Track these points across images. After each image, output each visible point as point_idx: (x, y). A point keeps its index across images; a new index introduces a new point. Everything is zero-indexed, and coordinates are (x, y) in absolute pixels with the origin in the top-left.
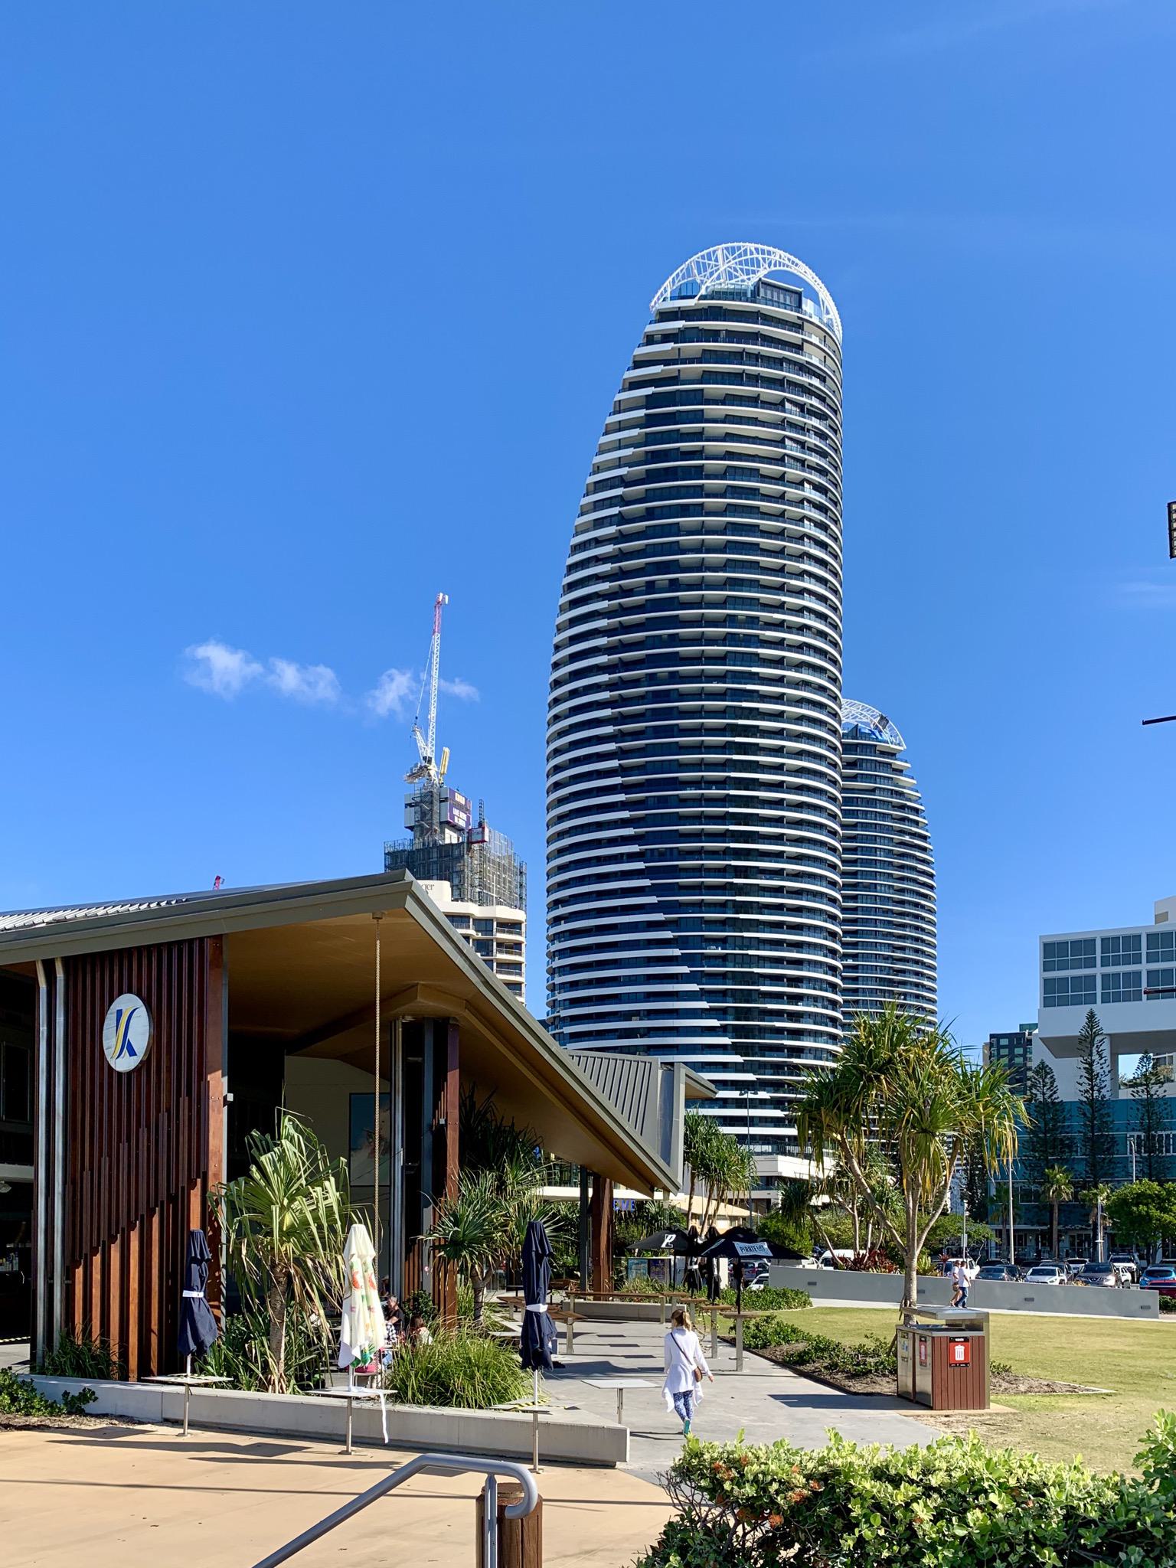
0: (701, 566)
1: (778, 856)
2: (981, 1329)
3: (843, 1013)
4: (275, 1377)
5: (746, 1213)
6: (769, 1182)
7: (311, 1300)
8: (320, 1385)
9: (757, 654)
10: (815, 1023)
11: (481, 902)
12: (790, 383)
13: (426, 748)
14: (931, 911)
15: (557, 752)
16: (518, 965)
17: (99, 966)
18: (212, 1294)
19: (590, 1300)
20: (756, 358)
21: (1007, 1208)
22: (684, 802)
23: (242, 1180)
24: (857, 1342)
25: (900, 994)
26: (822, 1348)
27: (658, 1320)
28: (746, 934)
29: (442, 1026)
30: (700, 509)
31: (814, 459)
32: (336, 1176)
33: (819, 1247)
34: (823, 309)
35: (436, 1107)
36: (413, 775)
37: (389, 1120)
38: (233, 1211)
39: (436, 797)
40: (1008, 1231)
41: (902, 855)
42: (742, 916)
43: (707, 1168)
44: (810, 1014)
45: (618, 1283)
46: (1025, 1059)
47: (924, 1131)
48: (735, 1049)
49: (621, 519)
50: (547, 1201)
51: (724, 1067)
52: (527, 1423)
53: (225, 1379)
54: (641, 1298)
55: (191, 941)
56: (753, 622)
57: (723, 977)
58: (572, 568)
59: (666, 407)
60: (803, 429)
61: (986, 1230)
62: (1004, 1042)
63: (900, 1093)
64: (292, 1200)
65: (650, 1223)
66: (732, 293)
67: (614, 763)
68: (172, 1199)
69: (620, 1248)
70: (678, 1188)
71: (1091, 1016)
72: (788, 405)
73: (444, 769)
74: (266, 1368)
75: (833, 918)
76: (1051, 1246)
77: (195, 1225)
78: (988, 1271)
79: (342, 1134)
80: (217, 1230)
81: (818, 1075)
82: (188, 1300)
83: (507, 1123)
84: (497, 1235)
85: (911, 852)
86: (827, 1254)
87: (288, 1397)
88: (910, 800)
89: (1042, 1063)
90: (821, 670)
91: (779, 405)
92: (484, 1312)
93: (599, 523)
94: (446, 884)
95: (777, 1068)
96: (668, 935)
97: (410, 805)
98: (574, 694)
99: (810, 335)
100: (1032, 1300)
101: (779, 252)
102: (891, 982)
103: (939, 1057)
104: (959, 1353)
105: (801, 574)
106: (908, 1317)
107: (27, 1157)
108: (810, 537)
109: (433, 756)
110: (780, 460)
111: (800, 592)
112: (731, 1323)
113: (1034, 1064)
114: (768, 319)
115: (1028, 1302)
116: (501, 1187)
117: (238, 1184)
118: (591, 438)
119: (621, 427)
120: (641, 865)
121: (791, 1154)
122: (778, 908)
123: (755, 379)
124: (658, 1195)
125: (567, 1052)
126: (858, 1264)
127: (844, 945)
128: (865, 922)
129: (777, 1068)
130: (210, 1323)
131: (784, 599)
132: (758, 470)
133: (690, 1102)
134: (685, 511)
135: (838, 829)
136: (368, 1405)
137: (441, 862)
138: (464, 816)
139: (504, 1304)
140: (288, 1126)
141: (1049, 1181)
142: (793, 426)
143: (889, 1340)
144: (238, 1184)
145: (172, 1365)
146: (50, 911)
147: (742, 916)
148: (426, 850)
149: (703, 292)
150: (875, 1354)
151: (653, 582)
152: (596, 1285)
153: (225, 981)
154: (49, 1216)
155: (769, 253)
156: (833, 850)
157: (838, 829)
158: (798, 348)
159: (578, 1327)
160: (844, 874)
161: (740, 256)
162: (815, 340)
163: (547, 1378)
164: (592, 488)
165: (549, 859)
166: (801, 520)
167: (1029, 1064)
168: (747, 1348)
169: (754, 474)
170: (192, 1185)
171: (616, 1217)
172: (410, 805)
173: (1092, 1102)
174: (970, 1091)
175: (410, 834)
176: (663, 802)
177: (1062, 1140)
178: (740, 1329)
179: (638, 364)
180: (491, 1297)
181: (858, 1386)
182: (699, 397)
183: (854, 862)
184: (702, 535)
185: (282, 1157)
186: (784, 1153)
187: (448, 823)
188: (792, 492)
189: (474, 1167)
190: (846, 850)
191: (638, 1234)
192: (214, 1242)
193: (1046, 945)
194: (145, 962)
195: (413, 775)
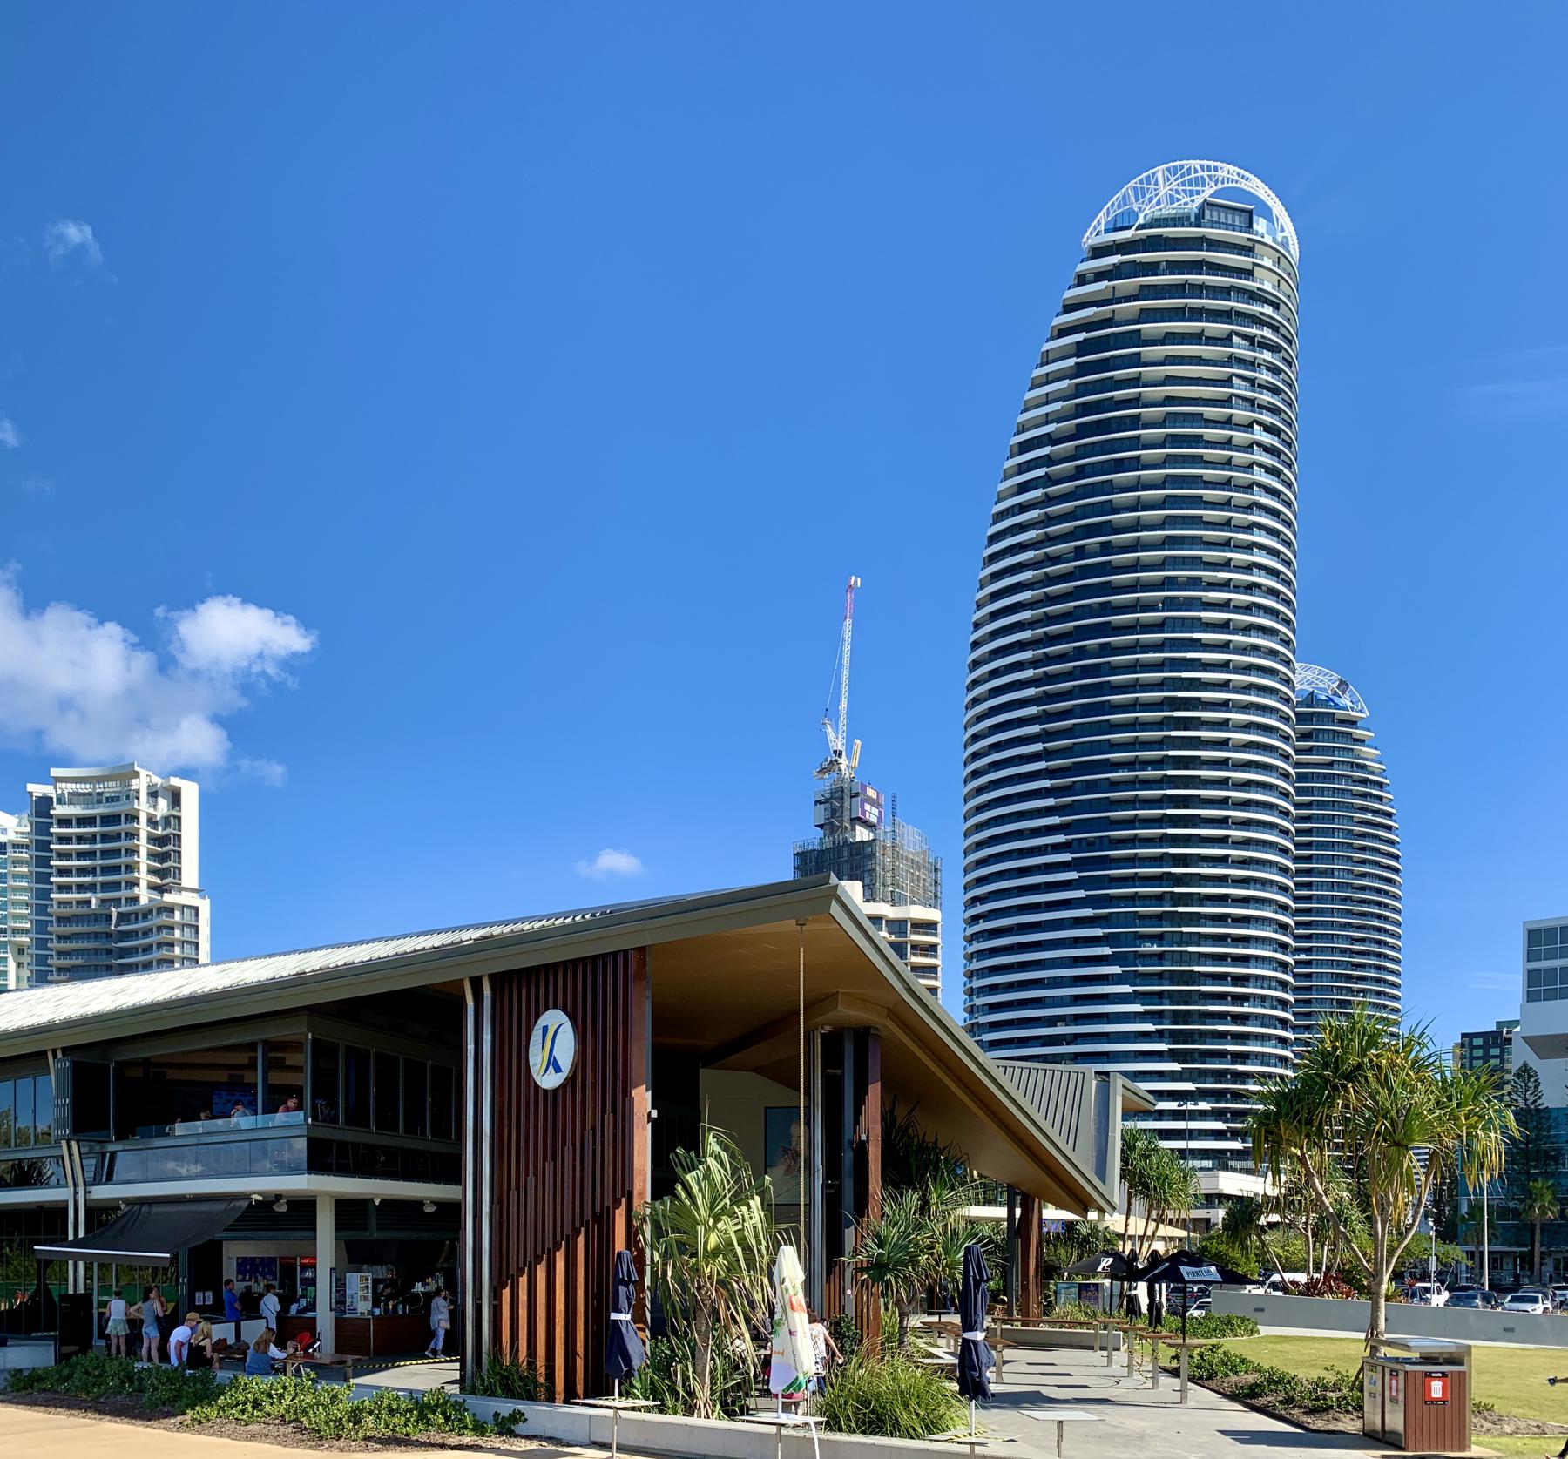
0: (1137, 526)
2: (1462, 1364)
3: (1294, 1014)
4: (701, 1402)
5: (1184, 1234)
6: (1212, 1199)
7: (736, 1322)
8: (745, 1410)
9: (1200, 619)
10: (1262, 1026)
11: (895, 901)
12: (1238, 313)
13: (837, 741)
14: (1395, 897)
15: (976, 738)
16: (934, 969)
17: (525, 980)
18: (638, 1317)
19: (1018, 1326)
20: (1200, 290)
21: (1481, 1223)
22: (1115, 785)
23: (667, 1199)
24: (1314, 1374)
25: (1359, 991)
26: (1276, 1380)
27: (1091, 1348)
28: (1185, 929)
29: (863, 1036)
30: (1136, 464)
31: (1265, 397)
32: (762, 1195)
33: (1268, 1271)
34: (1279, 228)
35: (857, 1122)
36: (822, 771)
37: (809, 1136)
38: (658, 1232)
40: (1482, 1253)
41: (1363, 836)
42: (1181, 909)
43: (1146, 1186)
44: (1257, 1016)
45: (1048, 1308)
46: (1503, 1061)
47: (1397, 1144)
48: (1172, 1056)
49: (1048, 480)
50: (972, 1222)
51: (1161, 1075)
52: (963, 1455)
53: (652, 1403)
54: (1074, 1324)
55: (615, 954)
56: (1194, 583)
57: (1160, 977)
58: (993, 539)
59: (1100, 351)
60: (1253, 364)
61: (1457, 1252)
62: (1478, 1042)
63: (1369, 1102)
64: (717, 1219)
65: (1081, 1246)
66: (1173, 219)
67: (1038, 747)
68: (597, 1219)
69: (1049, 1271)
70: (1114, 1208)
73: (855, 763)
74: (691, 1394)
75: (1284, 908)
76: (1531, 1269)
77: (620, 1245)
78: (1458, 1297)
79: (766, 1149)
80: (641, 1252)
81: (1276, 1084)
82: (615, 1321)
83: (930, 1139)
84: (923, 1258)
85: (1373, 833)
86: (1276, 1278)
87: (713, 1422)
88: (1373, 773)
89: (1525, 1065)
91: (1226, 340)
92: (909, 1338)
93: (1024, 488)
94: (858, 884)
97: (820, 802)
98: (995, 674)
100: (1512, 1330)
102: (1349, 978)
103: (1415, 1062)
104: (1436, 1389)
106: (1374, 1349)
107: (456, 1178)
109: (843, 749)
110: (1225, 402)
111: (1248, 547)
112: (1172, 1352)
113: (1514, 1065)
114: (1214, 245)
115: (1508, 1333)
116: (924, 1207)
117: (663, 1204)
118: (1017, 388)
119: (1048, 379)
120: (1067, 857)
121: (1234, 1170)
123: (1198, 314)
124: (1092, 1216)
125: (986, 1058)
126: (1311, 1289)
127: (1296, 938)
128: (1320, 912)
129: (1220, 1076)
130: (639, 1345)
131: (1230, 555)
133: (1126, 1116)
134: (1119, 466)
135: (1291, 809)
136: (801, 1433)
137: (857, 862)
138: (875, 811)
139: (928, 1328)
140: (712, 1144)
141: (1530, 1196)
142: (1241, 362)
143: (1353, 1373)
144: (663, 1204)
145: (598, 1387)
146: (476, 927)
147: (1181, 909)
148: (837, 849)
149: (1141, 221)
150: (1336, 1388)
152: (1025, 1311)
153: (649, 994)
154: (477, 1238)
155: (1216, 169)
156: (1285, 832)
157: (1291, 809)
158: (1248, 274)
159: (1008, 1354)
160: (1297, 859)
161: (1183, 176)
162: (1267, 262)
163: (984, 1408)
164: (1016, 449)
165: (966, 853)
166: (1249, 467)
167: (1507, 1066)
168: (1192, 1379)
169: (1198, 419)
170: (617, 1204)
171: (1043, 1239)
172: (820, 802)
174: (1450, 1100)
175: (820, 833)
176: (1092, 787)
177: (1546, 1152)
178: (1184, 1359)
179: (1068, 308)
180: (915, 1321)
181: (1318, 1423)
182: (1136, 339)
183: (1309, 845)
184: (1137, 495)
185: (708, 1175)
186: (1226, 1168)
188: (1240, 436)
189: (896, 1187)
190: (1299, 832)
191: (1066, 1256)
192: (639, 1261)
193: (1530, 932)
194: (570, 975)
195: (822, 771)
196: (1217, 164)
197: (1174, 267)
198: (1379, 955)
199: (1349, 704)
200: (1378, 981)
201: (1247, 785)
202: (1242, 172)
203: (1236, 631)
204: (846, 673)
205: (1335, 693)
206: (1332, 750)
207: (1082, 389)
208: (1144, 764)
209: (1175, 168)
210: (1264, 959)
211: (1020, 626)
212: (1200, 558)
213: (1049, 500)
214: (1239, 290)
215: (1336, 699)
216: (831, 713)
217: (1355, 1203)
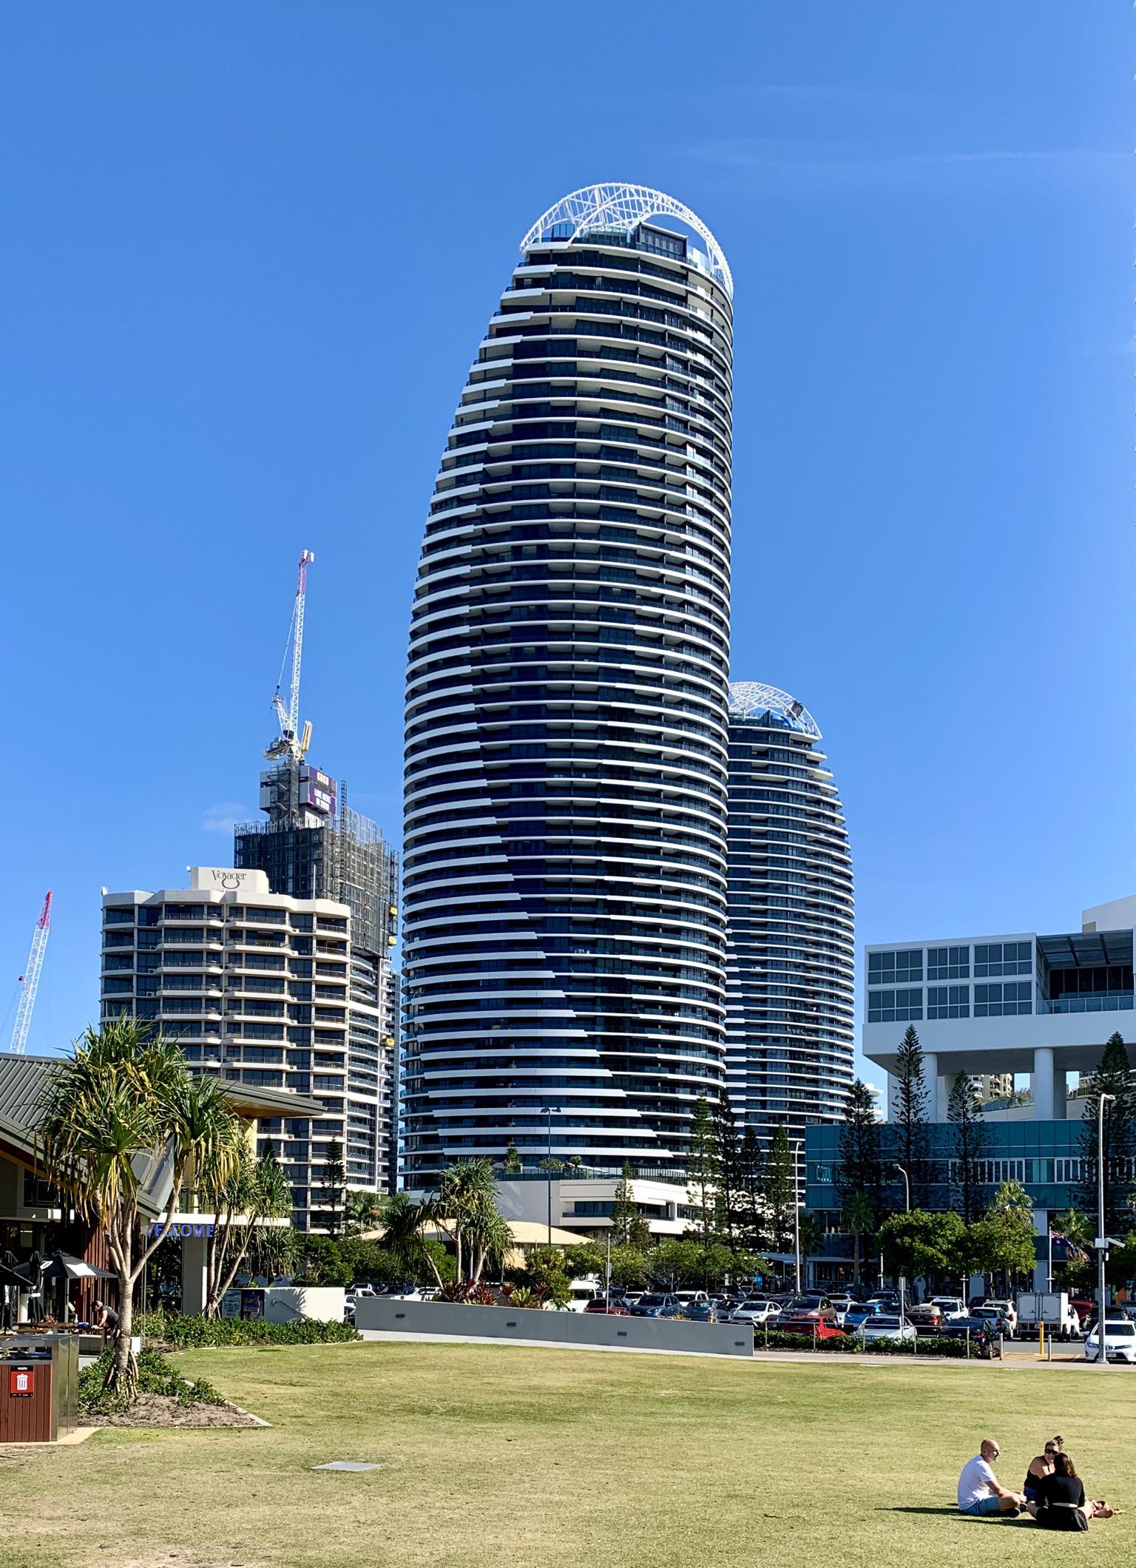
0: (572, 532)
1: (654, 852)
9: (634, 631)
12: (672, 337)
14: (848, 916)
15: (415, 730)
20: (635, 309)
28: (617, 937)
30: (572, 471)
31: (700, 421)
34: (709, 259)
36: (272, 751)
39: (294, 776)
41: (817, 854)
42: (613, 917)
51: (592, 1082)
56: (628, 595)
59: (534, 356)
60: (686, 387)
71: (911, 1033)
72: (668, 361)
88: (826, 795)
90: (703, 651)
91: (660, 361)
93: (461, 480)
95: (652, 1083)
96: (532, 936)
97: (266, 784)
98: (433, 666)
99: (695, 286)
101: (661, 195)
102: (803, 993)
104: (22, 1382)
105: (682, 546)
108: (693, 505)
110: (659, 421)
111: (682, 565)
115: (511, 1328)
118: (440, 384)
119: (486, 376)
122: (653, 910)
123: (632, 332)
132: (635, 430)
134: (555, 471)
138: (327, 798)
142: (675, 384)
147: (613, 917)
148: (280, 836)
149: (577, 234)
151: (520, 547)
158: (682, 300)
161: (619, 197)
162: (701, 291)
164: (454, 441)
166: (682, 486)
172: (266, 784)
173: (907, 1126)
176: (529, 790)
179: (506, 309)
182: (571, 348)
184: (573, 497)
186: (636, 1177)
187: (308, 805)
195: (272, 751)
196: (652, 191)
197: (610, 284)
198: (831, 971)
200: (831, 996)
201: (679, 799)
202: (676, 202)
204: (298, 650)
205: (790, 715)
206: (785, 770)
207: (519, 390)
208: (579, 771)
209: (611, 188)
214: (673, 314)
215: (790, 720)
216: (281, 691)
217: (441, 1221)
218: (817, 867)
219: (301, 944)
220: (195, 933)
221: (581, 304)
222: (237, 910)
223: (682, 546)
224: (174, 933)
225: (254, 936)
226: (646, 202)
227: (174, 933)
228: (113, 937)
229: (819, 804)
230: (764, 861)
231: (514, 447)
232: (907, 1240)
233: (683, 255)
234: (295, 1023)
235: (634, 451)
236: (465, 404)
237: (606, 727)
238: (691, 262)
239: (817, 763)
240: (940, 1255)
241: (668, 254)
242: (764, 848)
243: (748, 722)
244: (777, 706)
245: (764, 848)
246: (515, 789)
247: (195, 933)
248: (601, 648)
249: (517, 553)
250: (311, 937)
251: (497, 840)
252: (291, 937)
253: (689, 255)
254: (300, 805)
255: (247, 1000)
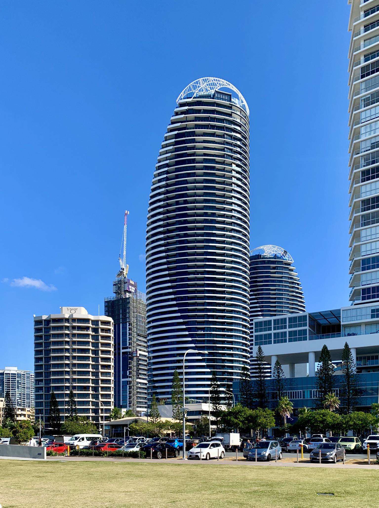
1: (223, 298)
20: (213, 119)
30: (194, 175)
34: (240, 101)
41: (293, 300)
48: (208, 367)
56: (213, 215)
57: (203, 342)
59: (182, 138)
67: (166, 266)
88: (296, 280)
93: (160, 181)
96: (184, 327)
97: (115, 285)
101: (222, 80)
105: (231, 197)
108: (235, 184)
110: (223, 156)
118: (156, 150)
119: (167, 146)
123: (213, 127)
131: (224, 206)
134: (189, 175)
142: (228, 143)
149: (195, 95)
151: (178, 201)
158: (230, 115)
164: (157, 168)
172: (115, 285)
176: (183, 280)
182: (193, 134)
184: (195, 186)
196: (219, 79)
197: (206, 111)
199: (287, 259)
201: (232, 281)
202: (227, 82)
203: (227, 231)
204: (125, 243)
205: (283, 255)
207: (177, 149)
208: (198, 273)
209: (206, 79)
210: (237, 336)
211: (160, 226)
212: (215, 206)
213: (167, 185)
216: (121, 256)
218: (293, 304)
219: (95, 330)
220: (61, 328)
221: (197, 119)
222: (74, 320)
223: (231, 197)
224: (55, 328)
225: (80, 328)
226: (218, 83)
227: (55, 328)
228: (37, 330)
229: (293, 283)
230: (275, 303)
231: (176, 168)
232: (229, 417)
233: (230, 101)
234: (94, 356)
235: (214, 167)
236: (161, 155)
237: (207, 258)
238: (233, 102)
239: (293, 270)
240: (239, 422)
241: (225, 100)
242: (275, 298)
243: (269, 258)
244: (279, 252)
245: (275, 298)
246: (178, 280)
247: (61, 328)
248: (205, 233)
249: (177, 203)
250: (98, 328)
251: (173, 296)
252: (92, 328)
253: (232, 99)
254: (125, 291)
255: (78, 349)
